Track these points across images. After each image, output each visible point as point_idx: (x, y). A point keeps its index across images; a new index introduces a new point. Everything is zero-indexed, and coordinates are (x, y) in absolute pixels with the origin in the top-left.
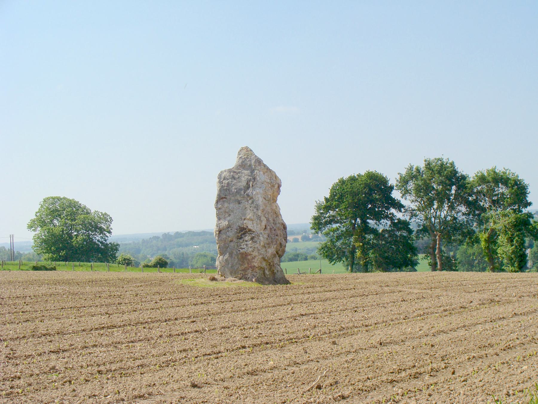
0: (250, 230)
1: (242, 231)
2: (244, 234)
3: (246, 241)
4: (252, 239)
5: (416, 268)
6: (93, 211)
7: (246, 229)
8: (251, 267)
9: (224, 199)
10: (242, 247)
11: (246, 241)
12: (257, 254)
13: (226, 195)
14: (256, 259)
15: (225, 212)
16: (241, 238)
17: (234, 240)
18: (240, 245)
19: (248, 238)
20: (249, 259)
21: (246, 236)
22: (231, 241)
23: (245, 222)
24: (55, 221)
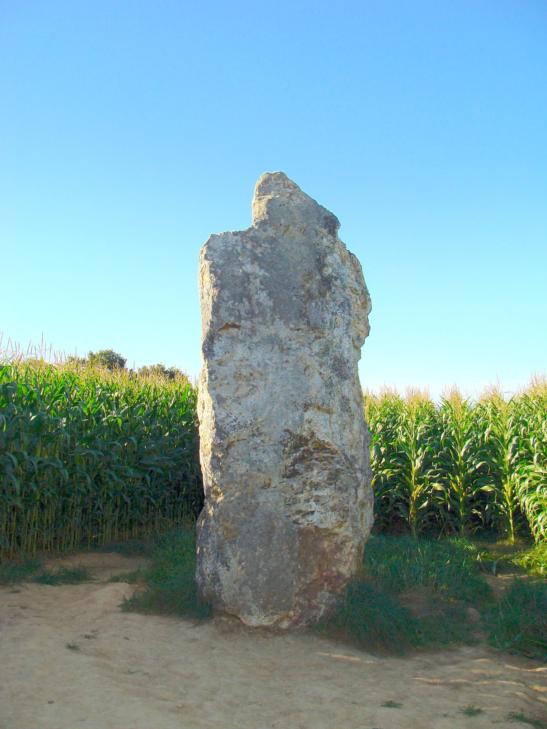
0: (321, 447)
1: (296, 448)
2: (301, 459)
3: (316, 486)
4: (333, 477)
5: (382, 536)
6: (403, 395)
7: (306, 441)
8: (328, 579)
9: (234, 331)
10: (303, 507)
11: (316, 486)
12: (349, 533)
13: (239, 318)
14: (346, 550)
15: (238, 376)
16: (294, 474)
17: (276, 481)
18: (295, 501)
19: (316, 475)
20: (324, 552)
21: (309, 468)
22: (266, 486)
23: (308, 415)
24: (404, 440)
